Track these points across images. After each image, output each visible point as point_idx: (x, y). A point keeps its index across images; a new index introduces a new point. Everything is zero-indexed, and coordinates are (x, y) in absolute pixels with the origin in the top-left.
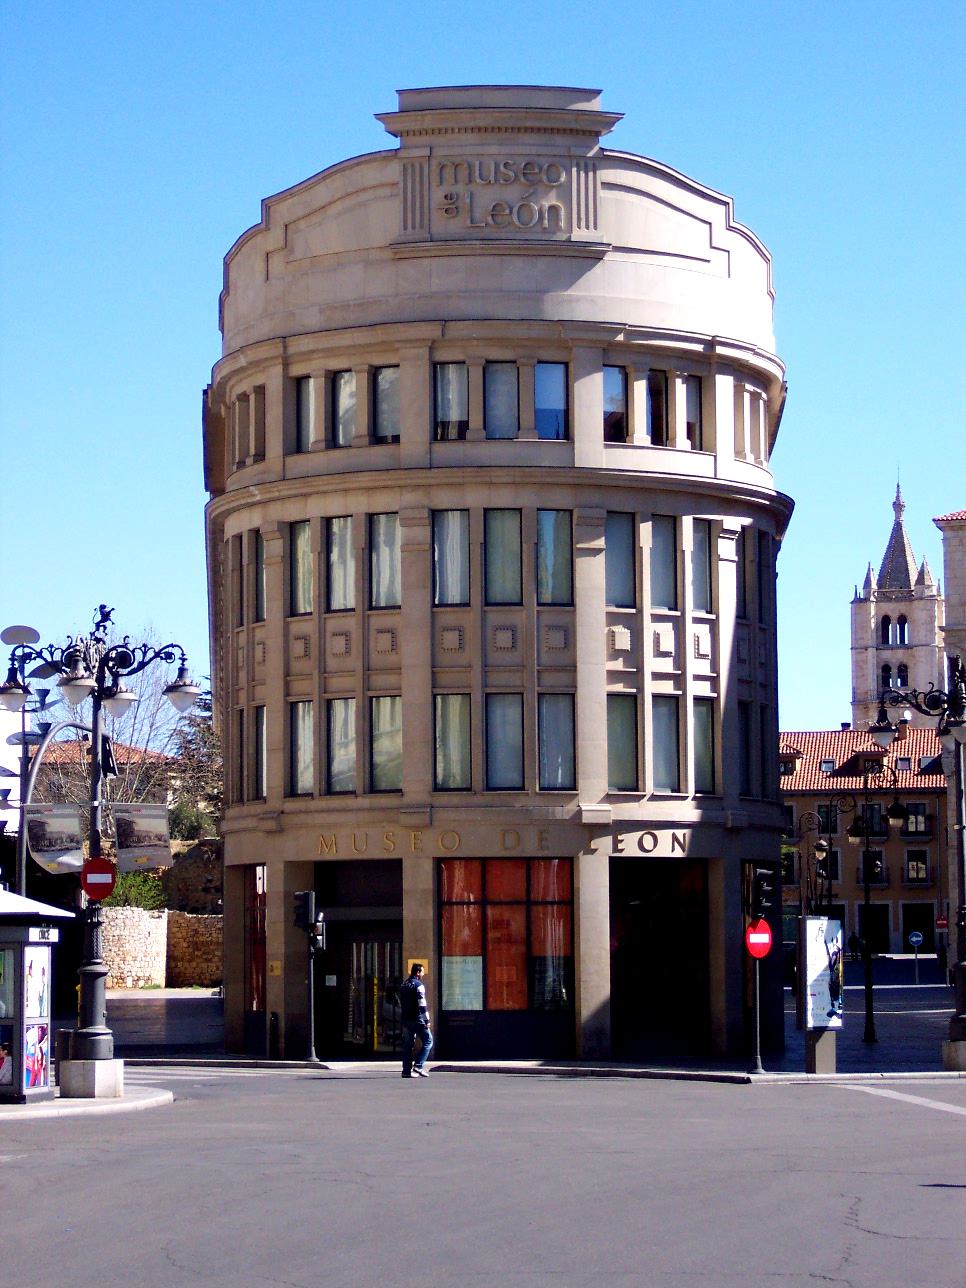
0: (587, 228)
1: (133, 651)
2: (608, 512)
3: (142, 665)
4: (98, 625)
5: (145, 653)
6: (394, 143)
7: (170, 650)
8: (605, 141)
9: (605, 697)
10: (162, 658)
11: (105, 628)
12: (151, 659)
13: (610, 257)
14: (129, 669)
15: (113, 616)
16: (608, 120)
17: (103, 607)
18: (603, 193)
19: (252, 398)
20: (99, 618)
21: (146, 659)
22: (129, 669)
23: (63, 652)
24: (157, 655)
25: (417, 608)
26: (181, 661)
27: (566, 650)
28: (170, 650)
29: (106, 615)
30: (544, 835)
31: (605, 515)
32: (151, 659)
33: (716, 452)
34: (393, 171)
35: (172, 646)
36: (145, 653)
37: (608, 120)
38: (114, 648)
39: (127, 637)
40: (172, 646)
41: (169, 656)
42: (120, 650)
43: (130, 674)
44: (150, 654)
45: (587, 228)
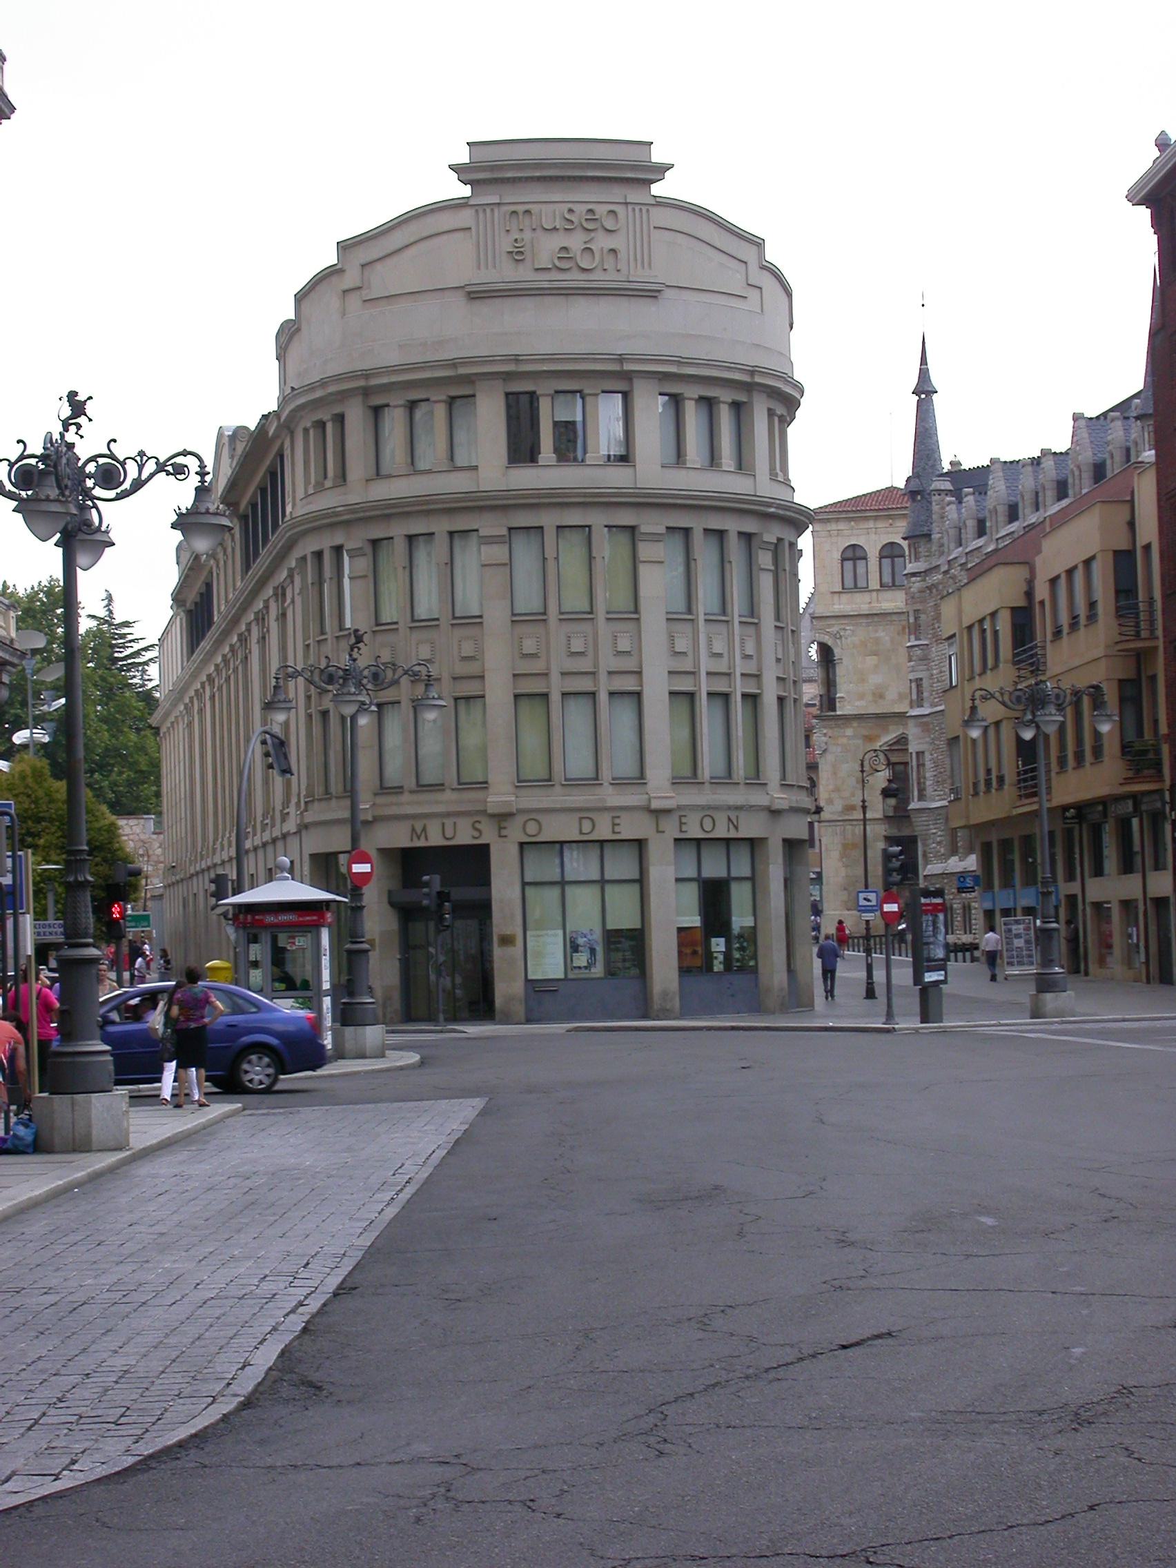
0: (643, 267)
1: (123, 464)
2: (667, 528)
3: (138, 485)
4: (66, 425)
5: (141, 467)
6: (466, 191)
7: (180, 460)
8: (657, 189)
9: (667, 695)
10: (168, 473)
11: (79, 426)
12: (152, 476)
13: (669, 293)
14: (119, 490)
15: (89, 408)
16: (663, 169)
17: (72, 395)
18: (656, 234)
19: (329, 426)
20: (66, 412)
21: (144, 476)
22: (119, 490)
23: (11, 465)
24: (161, 467)
25: (496, 616)
26: (198, 478)
27: (745, 285)
28: (180, 460)
29: (77, 407)
30: (617, 821)
31: (664, 531)
32: (152, 476)
33: (754, 471)
34: (465, 218)
35: (185, 453)
36: (141, 467)
37: (663, 169)
38: (93, 459)
39: (115, 441)
40: (185, 453)
41: (179, 470)
42: (101, 461)
43: (119, 497)
44: (150, 467)
45: (643, 267)
